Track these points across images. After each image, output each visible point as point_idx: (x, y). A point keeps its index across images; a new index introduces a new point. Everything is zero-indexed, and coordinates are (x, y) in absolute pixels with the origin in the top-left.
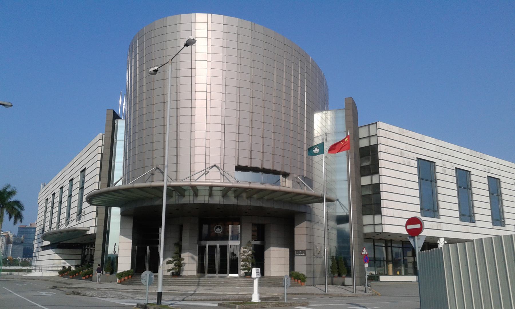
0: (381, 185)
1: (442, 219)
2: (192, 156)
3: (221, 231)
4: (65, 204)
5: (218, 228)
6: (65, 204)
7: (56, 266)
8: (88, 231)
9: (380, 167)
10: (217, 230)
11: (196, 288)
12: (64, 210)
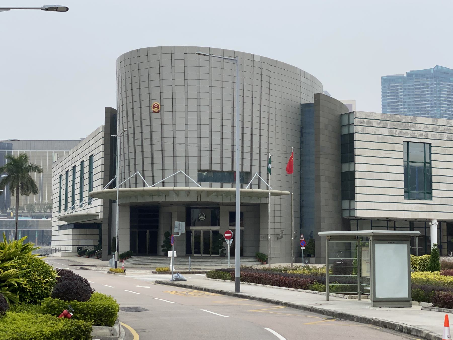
0: (355, 172)
1: (435, 200)
2: (173, 156)
3: (205, 218)
4: (78, 186)
5: (202, 216)
6: (78, 186)
7: (75, 246)
8: (386, 229)
9: (355, 147)
10: (200, 217)
11: (4, 287)
12: (78, 191)
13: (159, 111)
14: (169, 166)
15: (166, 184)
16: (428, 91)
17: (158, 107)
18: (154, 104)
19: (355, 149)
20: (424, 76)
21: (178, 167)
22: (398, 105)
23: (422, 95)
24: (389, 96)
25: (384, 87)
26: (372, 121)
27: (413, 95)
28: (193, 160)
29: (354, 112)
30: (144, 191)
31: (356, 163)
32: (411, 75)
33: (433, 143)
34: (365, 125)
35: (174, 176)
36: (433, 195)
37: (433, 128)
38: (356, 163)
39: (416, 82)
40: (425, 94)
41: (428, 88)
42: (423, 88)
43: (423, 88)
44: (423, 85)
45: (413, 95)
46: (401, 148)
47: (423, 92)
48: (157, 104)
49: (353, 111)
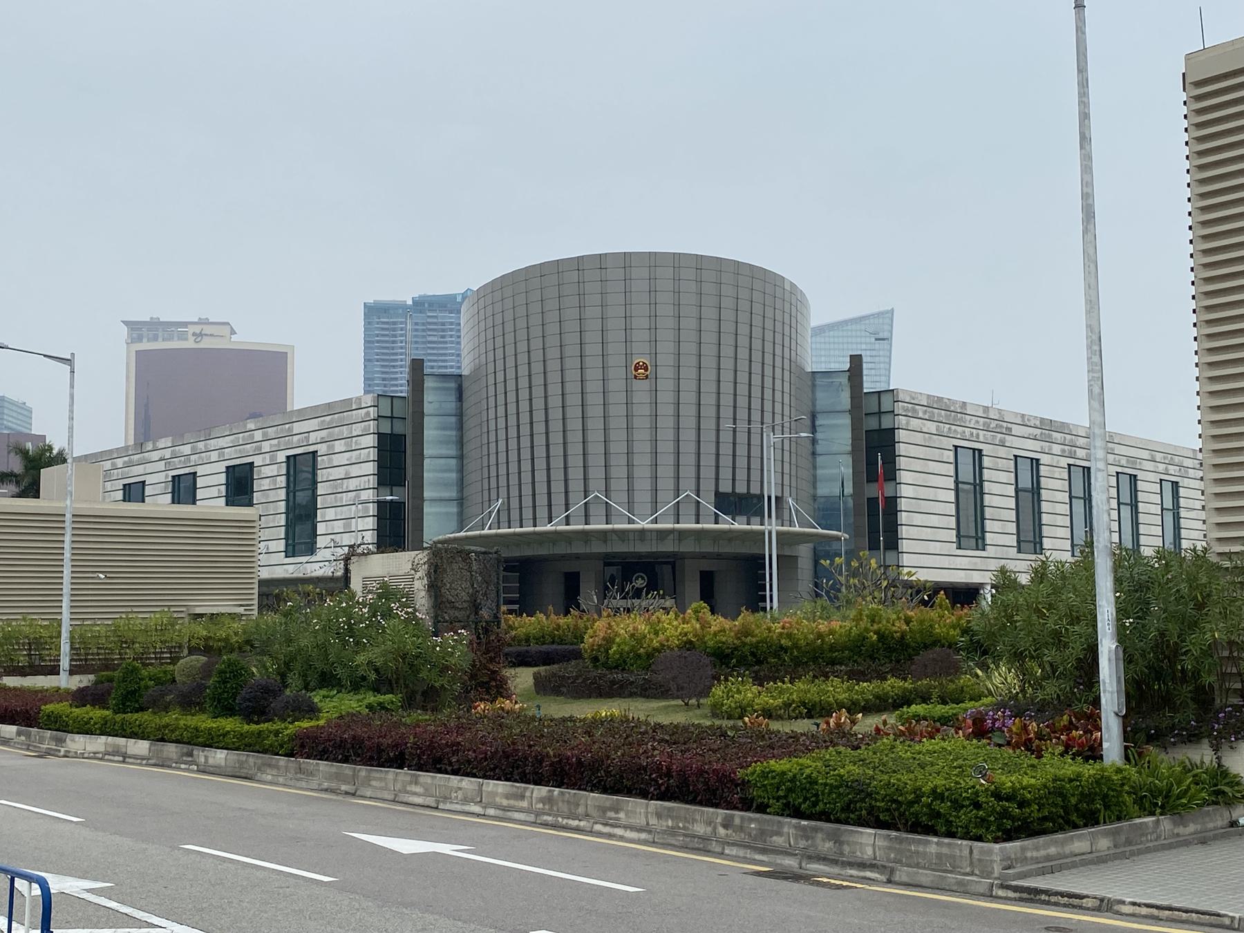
0: (898, 499)
13: (647, 377)
14: (576, 486)
15: (571, 519)
16: (451, 336)
17: (646, 369)
18: (638, 363)
19: (897, 458)
20: (445, 307)
21: (592, 484)
22: (396, 360)
23: (440, 342)
24: (378, 342)
25: (369, 323)
26: (917, 407)
27: (424, 343)
28: (708, 473)
29: (893, 390)
30: (535, 533)
31: (900, 483)
32: (421, 304)
33: (986, 449)
34: (910, 414)
35: (586, 503)
36: (988, 542)
37: (984, 424)
38: (900, 483)
39: (429, 317)
40: (446, 343)
41: (451, 330)
42: (443, 330)
43: (443, 330)
44: (443, 324)
45: (424, 343)
46: (950, 456)
47: (443, 337)
48: (644, 363)
49: (891, 388)
